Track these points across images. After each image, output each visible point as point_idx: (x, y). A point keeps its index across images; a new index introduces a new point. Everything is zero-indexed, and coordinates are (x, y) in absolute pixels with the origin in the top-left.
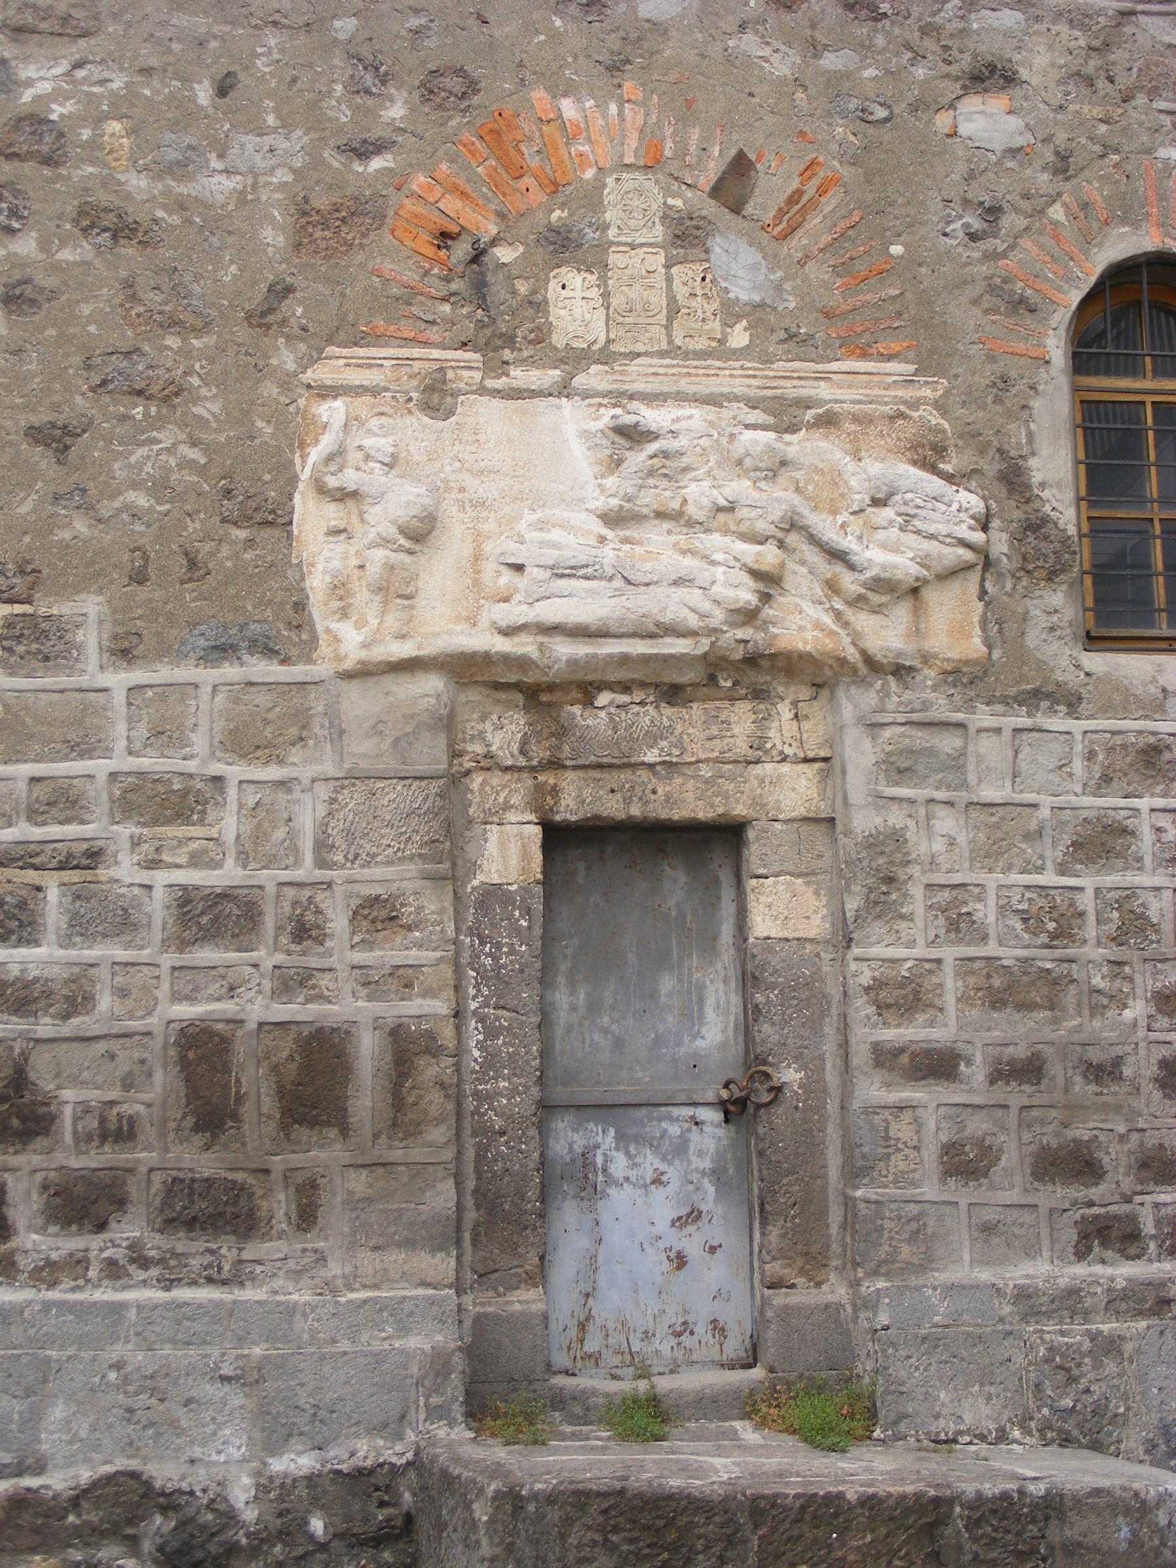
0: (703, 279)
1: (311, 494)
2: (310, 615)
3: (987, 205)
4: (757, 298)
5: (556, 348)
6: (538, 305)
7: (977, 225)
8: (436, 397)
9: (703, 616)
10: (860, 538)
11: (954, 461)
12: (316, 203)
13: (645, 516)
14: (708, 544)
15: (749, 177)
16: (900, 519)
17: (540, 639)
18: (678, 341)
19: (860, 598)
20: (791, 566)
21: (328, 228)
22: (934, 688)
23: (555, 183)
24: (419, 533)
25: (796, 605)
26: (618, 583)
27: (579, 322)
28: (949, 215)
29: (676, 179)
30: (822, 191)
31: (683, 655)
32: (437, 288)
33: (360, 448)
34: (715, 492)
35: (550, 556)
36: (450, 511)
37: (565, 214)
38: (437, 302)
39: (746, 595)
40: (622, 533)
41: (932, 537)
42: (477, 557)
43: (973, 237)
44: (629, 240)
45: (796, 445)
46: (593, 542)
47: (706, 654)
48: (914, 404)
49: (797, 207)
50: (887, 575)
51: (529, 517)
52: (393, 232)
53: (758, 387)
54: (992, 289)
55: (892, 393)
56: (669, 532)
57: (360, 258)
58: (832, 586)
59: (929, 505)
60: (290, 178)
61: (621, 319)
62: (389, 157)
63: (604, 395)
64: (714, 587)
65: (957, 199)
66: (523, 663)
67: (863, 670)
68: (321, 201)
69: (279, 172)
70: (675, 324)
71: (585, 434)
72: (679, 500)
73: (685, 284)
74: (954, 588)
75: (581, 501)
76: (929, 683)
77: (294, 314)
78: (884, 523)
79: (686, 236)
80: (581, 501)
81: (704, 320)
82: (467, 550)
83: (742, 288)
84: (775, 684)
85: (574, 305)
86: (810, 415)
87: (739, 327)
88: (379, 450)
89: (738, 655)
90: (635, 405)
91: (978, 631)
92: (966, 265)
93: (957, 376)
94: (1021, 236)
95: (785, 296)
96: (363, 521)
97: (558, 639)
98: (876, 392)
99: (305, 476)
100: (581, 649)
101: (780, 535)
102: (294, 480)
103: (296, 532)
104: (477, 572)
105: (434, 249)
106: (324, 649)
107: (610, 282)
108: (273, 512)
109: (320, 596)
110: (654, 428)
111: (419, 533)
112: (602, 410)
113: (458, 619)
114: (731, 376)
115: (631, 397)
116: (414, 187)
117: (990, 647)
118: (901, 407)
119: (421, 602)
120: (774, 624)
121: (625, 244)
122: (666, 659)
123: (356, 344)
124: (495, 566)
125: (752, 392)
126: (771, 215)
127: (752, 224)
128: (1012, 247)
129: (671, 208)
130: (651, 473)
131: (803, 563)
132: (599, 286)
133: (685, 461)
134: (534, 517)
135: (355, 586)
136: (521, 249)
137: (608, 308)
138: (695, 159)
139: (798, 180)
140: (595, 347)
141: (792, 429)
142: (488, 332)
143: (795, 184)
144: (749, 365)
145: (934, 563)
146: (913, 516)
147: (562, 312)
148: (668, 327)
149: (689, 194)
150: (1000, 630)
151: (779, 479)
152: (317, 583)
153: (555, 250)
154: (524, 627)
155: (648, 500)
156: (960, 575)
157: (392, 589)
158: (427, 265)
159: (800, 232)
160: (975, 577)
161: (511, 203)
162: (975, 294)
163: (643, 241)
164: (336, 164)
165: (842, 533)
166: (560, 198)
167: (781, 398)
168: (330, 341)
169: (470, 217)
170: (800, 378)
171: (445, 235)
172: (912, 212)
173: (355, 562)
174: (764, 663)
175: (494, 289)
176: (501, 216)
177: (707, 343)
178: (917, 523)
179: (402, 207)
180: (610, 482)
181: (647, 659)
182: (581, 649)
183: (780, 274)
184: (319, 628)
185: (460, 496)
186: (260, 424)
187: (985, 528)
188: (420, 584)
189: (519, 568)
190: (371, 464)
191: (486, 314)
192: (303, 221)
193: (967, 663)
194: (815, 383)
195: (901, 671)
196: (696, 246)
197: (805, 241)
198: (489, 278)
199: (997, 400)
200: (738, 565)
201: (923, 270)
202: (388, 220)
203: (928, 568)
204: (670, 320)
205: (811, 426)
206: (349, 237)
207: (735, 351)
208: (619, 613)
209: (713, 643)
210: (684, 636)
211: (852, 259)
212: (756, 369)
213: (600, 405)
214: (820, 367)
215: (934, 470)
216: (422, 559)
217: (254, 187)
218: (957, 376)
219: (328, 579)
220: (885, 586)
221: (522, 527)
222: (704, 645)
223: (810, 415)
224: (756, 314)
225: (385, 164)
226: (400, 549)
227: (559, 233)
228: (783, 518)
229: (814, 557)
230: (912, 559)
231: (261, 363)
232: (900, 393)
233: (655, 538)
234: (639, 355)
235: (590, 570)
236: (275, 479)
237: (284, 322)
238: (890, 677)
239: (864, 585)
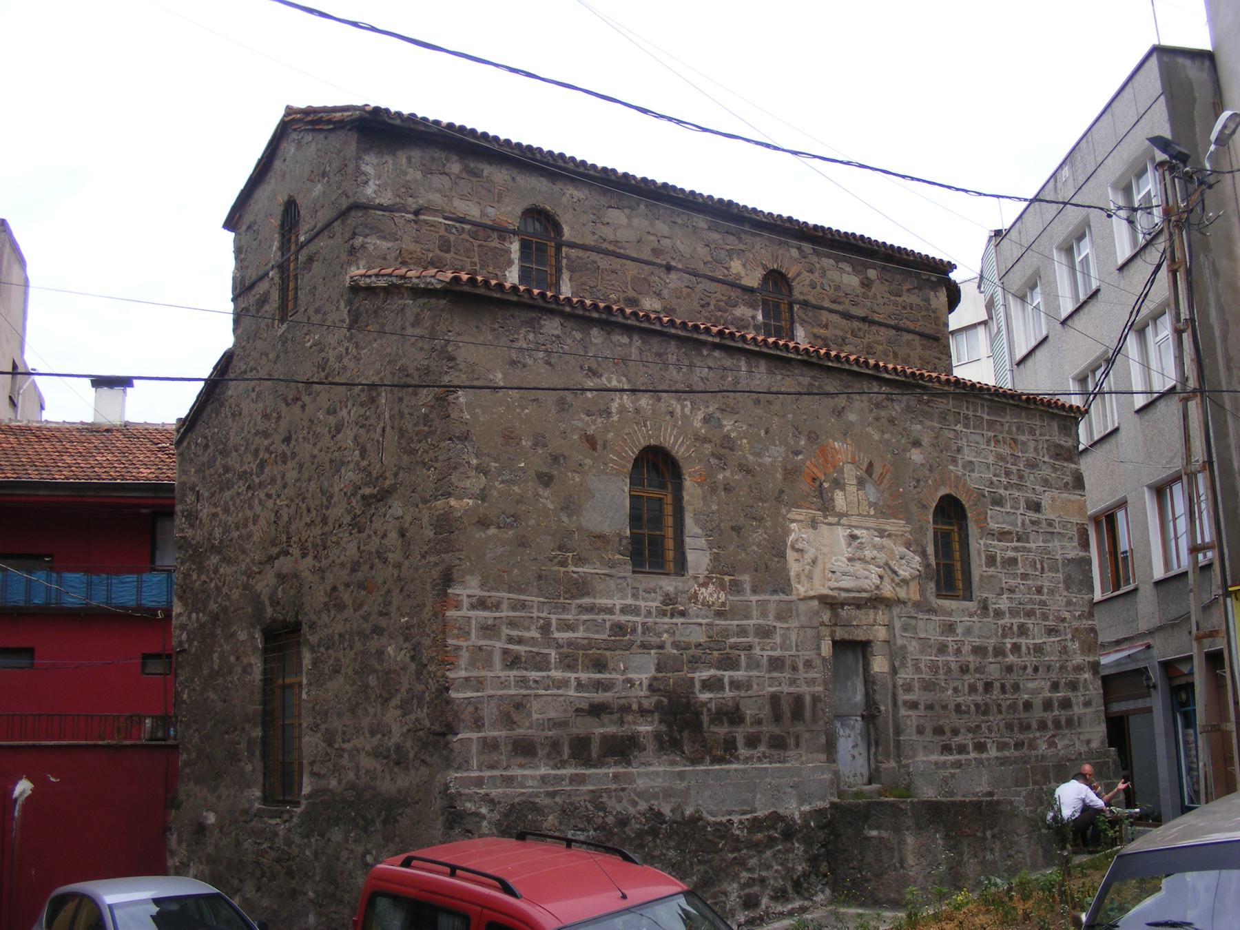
106: (794, 592)
152: (792, 574)
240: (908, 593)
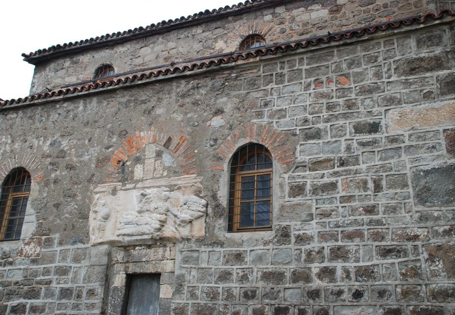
6: (132, 172)
12: (100, 159)
17: (123, 237)
24: (106, 218)
26: (136, 225)
30: (183, 142)
32: (116, 171)
39: (158, 226)
41: (193, 210)
42: (116, 222)
43: (212, 146)
48: (195, 183)
75: (134, 209)
80: (134, 209)
86: (176, 187)
101: (166, 213)
111: (106, 218)
115: (145, 188)
125: (166, 184)
133: (151, 200)
141: (173, 191)
152: (91, 229)
155: (145, 208)
168: (99, 183)
171: (119, 161)
180: (139, 205)
181: (141, 240)
188: (106, 228)
193: (200, 237)
207: (164, 176)
208: (135, 231)
220: (183, 221)
223: (176, 187)
224: (169, 169)
226: (102, 221)
229: (171, 215)
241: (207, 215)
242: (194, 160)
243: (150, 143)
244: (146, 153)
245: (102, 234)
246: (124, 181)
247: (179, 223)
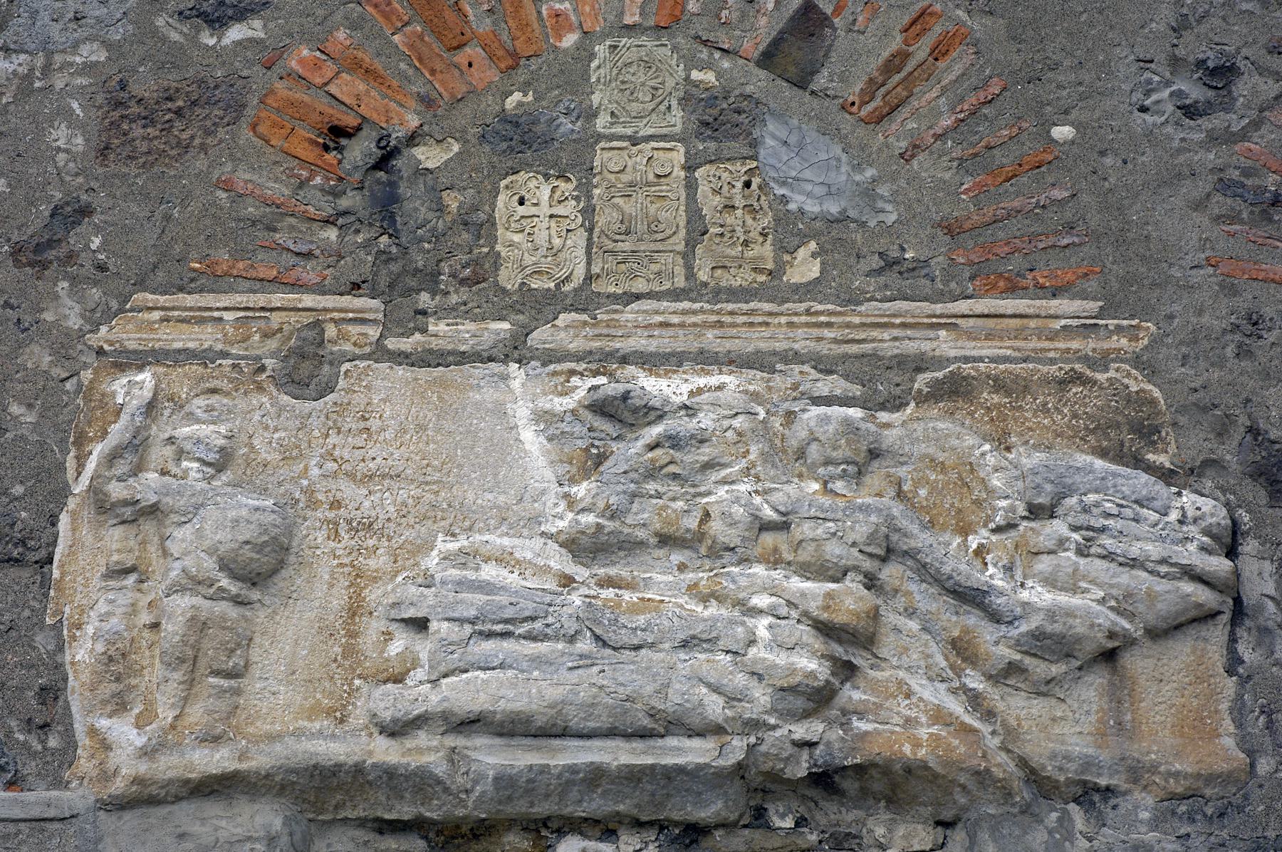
0: (747, 185)
1: (87, 514)
2: (67, 707)
3: (1211, 64)
4: (834, 208)
5: (504, 290)
6: (483, 228)
7: (1196, 93)
8: (306, 368)
9: (732, 699)
10: (1009, 569)
11: (1172, 448)
12: (136, 89)
13: (641, 544)
14: (743, 582)
15: (822, 37)
16: (1076, 536)
17: (451, 741)
18: (703, 276)
19: (1013, 669)
20: (891, 618)
21: (153, 123)
22: (1155, 824)
23: (515, 55)
24: (259, 569)
25: (901, 683)
26: (585, 645)
27: (543, 251)
28: (1149, 82)
29: (705, 43)
30: (939, 52)
31: (700, 767)
32: (321, 205)
33: (171, 440)
34: (758, 500)
35: (473, 603)
36: (312, 533)
37: (530, 98)
38: (315, 225)
39: (809, 664)
40: (601, 571)
41: (1133, 563)
42: (355, 610)
43: (1190, 111)
44: (629, 131)
45: (895, 427)
46: (551, 585)
47: (740, 766)
48: (1102, 361)
49: (897, 78)
50: (1057, 628)
51: (445, 545)
52: (254, 127)
53: (835, 341)
54: (1225, 186)
55: (1062, 345)
56: (682, 568)
57: (201, 163)
58: (962, 650)
59: (1128, 512)
60: (102, 56)
61: (610, 245)
62: (257, 23)
63: (578, 358)
64: (752, 652)
65: (1161, 57)
66: (422, 783)
67: (1024, 794)
68: (145, 85)
69: (85, 49)
70: (699, 250)
71: (544, 418)
72: (697, 514)
73: (717, 192)
74: (1182, 650)
75: (536, 520)
76: (1145, 815)
77: (87, 246)
78: (1050, 544)
79: (719, 124)
80: (536, 520)
81: (746, 243)
82: (339, 599)
83: (809, 195)
84: (870, 823)
85: (535, 224)
86: (922, 382)
87: (802, 253)
88: (199, 441)
89: (801, 770)
90: (631, 369)
91: (1228, 725)
92: (1179, 151)
93: (1171, 317)
94: (1270, 108)
95: (880, 204)
96: (165, 553)
97: (480, 741)
98: (1034, 344)
99: (80, 487)
100: (523, 758)
101: (868, 564)
102: (63, 493)
103: (56, 574)
104: (352, 635)
105: (318, 151)
106: (85, 764)
107: (597, 192)
108: (23, 542)
109: (85, 677)
110: (655, 403)
111: (259, 569)
112: (575, 380)
113: (313, 712)
114: (790, 325)
115: (624, 360)
116: (293, 64)
117: (1251, 753)
118: (1077, 366)
119: (254, 685)
120: (861, 715)
121: (621, 138)
122: (672, 775)
123: (181, 289)
124: (382, 625)
125: (824, 348)
126: (857, 90)
127: (827, 102)
128: (1256, 124)
129: (696, 84)
130: (652, 473)
131: (910, 612)
132: (577, 199)
133: (706, 453)
134: (453, 546)
135: (143, 658)
136: (456, 148)
137: (590, 230)
138: (735, 15)
139: (899, 38)
140: (567, 288)
141: (895, 404)
142: (395, 267)
143: (896, 43)
144: (820, 307)
145: (1141, 608)
146: (1103, 530)
147: (517, 238)
148: (688, 256)
149: (726, 64)
150: (1270, 725)
151: (867, 479)
152: (82, 653)
153: (511, 149)
154: (419, 722)
155: (644, 517)
156: (1192, 631)
157: (203, 662)
158: (305, 173)
159: (905, 112)
160: (1217, 633)
161: (443, 83)
162: (1197, 194)
163: (650, 131)
164: (175, 36)
165: (978, 563)
166: (522, 76)
167: (875, 356)
168: (141, 285)
169: (373, 103)
170: (904, 325)
171: (338, 132)
172: (1087, 77)
173: (145, 618)
174: (849, 785)
175: (408, 206)
176: (427, 102)
177: (750, 276)
178: (1107, 541)
179: (272, 92)
180: (581, 490)
181: (634, 776)
182: (523, 758)
183: (870, 173)
184: (79, 728)
185: (331, 515)
186: (15, 409)
187: (1232, 553)
188: (255, 654)
189: (420, 625)
190: (185, 464)
191: (401, 245)
192: (116, 114)
193: (1211, 779)
194: (931, 334)
195: (1090, 795)
196: (735, 137)
197: (912, 125)
198: (403, 189)
199: (1243, 352)
200: (794, 614)
201: (1108, 161)
202: (249, 111)
203: (1131, 616)
204: (691, 244)
205: (922, 399)
206: (184, 136)
207: (796, 288)
208: (584, 695)
209: (751, 748)
210: (701, 734)
211: (989, 148)
212: (831, 313)
213: (572, 372)
214: (938, 308)
215: (1137, 462)
216: (261, 615)
217: (47, 69)
218: (1171, 317)
219: (100, 648)
220: (1049, 643)
221: (431, 562)
222: (737, 748)
223: (922, 382)
224: (832, 234)
225: (250, 33)
226: (221, 595)
227: (517, 125)
228: (871, 538)
229: (923, 596)
230: (1102, 601)
231: (27, 319)
232: (1075, 345)
233: (660, 578)
234: (638, 297)
235: (538, 625)
236: (30, 493)
237: (71, 257)
238: (1072, 807)
239: (1017, 644)
240: (1118, 724)
241: (1239, 611)
242: (1058, 194)
243: (630, 29)
244: (596, 99)
245: (223, 705)
246: (402, 284)
247: (1006, 653)
